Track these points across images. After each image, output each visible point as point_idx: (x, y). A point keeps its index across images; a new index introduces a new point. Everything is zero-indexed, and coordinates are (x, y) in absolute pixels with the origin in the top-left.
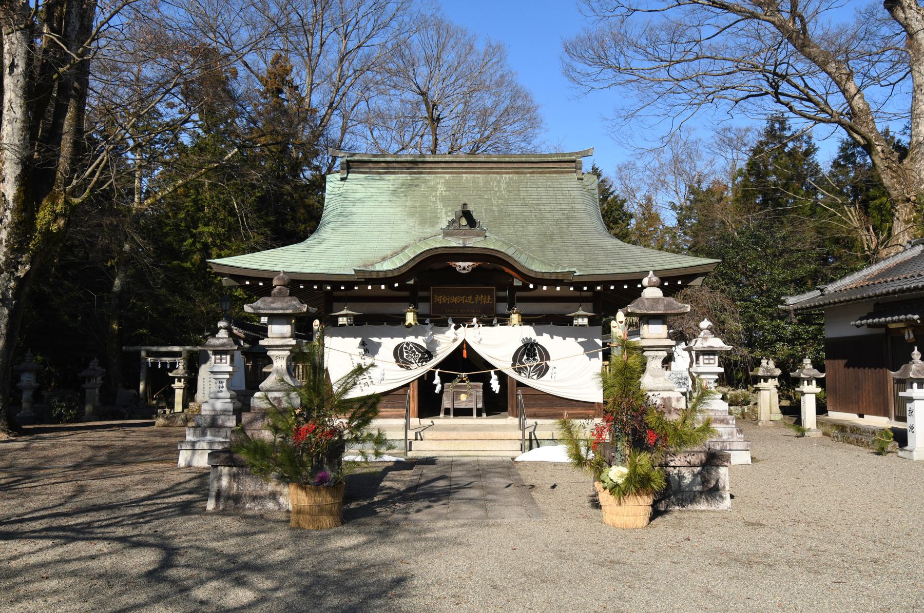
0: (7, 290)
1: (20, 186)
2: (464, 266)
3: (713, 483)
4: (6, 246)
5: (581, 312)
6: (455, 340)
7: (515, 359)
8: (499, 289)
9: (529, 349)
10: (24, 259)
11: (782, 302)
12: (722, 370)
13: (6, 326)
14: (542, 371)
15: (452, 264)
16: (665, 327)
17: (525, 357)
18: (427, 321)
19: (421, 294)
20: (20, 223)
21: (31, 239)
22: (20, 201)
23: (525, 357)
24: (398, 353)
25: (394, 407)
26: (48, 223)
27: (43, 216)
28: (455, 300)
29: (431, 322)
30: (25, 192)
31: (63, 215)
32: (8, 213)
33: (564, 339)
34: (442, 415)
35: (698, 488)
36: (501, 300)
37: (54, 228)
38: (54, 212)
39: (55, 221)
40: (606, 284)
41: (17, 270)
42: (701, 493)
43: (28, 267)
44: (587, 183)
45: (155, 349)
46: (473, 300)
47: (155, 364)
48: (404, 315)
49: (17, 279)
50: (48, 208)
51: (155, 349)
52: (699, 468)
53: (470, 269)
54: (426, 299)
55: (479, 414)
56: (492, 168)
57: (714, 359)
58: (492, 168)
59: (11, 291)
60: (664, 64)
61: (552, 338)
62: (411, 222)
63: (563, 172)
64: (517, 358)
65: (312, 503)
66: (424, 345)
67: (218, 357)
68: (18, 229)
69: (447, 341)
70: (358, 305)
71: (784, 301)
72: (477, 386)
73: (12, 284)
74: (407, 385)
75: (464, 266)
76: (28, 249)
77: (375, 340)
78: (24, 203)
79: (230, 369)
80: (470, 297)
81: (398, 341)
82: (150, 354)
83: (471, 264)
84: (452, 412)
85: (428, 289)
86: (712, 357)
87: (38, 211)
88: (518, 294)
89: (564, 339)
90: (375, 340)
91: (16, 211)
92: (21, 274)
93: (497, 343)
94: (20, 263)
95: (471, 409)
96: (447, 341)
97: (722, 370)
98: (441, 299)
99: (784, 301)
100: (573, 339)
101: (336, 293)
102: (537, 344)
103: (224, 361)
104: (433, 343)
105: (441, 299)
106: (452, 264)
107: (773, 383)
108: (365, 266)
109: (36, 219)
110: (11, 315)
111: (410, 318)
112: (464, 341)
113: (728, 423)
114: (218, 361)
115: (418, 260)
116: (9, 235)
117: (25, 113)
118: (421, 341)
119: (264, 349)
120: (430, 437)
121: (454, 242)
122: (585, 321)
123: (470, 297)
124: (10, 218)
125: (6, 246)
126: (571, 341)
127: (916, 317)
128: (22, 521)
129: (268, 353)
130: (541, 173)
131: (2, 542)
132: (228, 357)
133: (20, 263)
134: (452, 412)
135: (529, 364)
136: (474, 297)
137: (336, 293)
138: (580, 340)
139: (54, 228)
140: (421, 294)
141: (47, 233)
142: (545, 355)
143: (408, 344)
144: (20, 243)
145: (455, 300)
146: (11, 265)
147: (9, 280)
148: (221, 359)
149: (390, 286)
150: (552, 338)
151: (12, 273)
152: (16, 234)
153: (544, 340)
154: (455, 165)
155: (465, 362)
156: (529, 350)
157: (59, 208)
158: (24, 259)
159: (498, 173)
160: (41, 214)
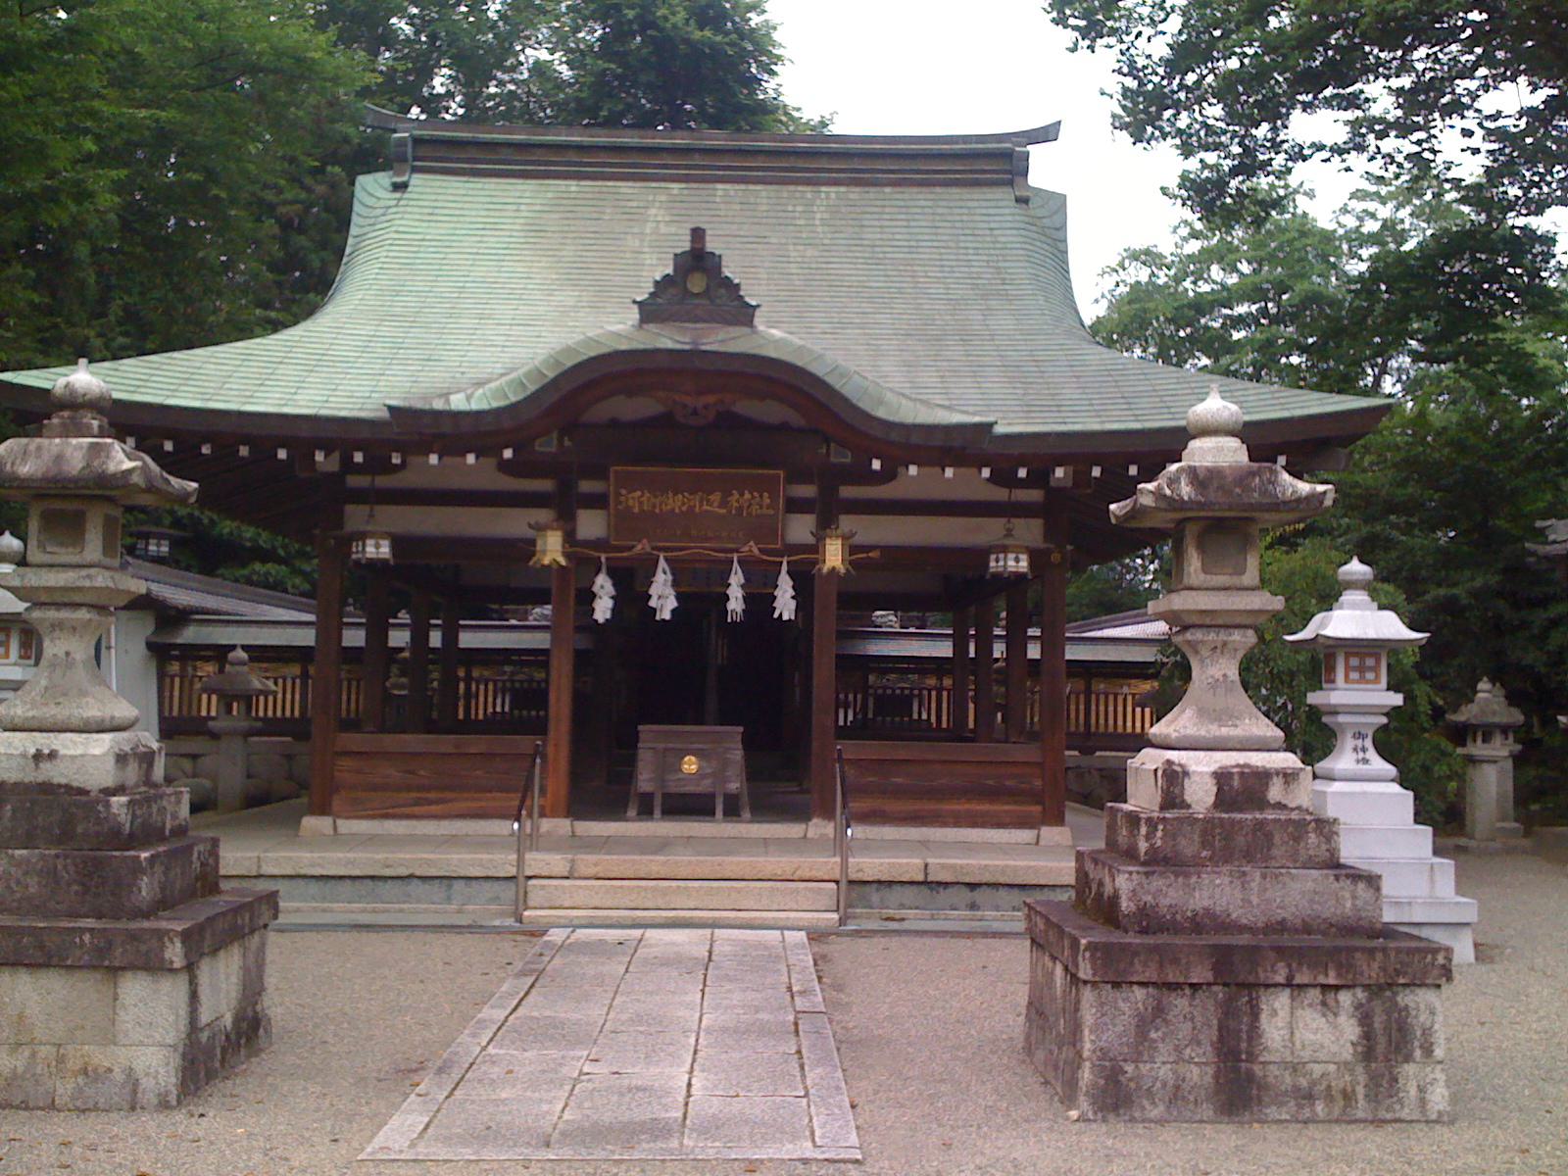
8: (794, 478)
11: (1540, 535)
12: (1397, 699)
19: (586, 486)
28: (675, 503)
34: (632, 813)
36: (795, 506)
44: (1040, 213)
46: (724, 504)
54: (597, 501)
55: (732, 811)
62: (567, 297)
71: (1542, 531)
80: (716, 497)
84: (658, 802)
85: (601, 474)
88: (847, 492)
95: (712, 796)
98: (637, 500)
99: (1542, 531)
107: (1501, 749)
108: (424, 398)
120: (592, 871)
123: (716, 497)
128: (766, 842)
131: (35, 996)
134: (658, 802)
136: (727, 494)
140: (586, 486)
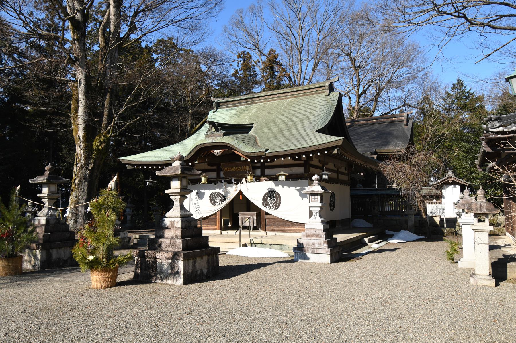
0: (86, 175)
1: (85, 132)
2: (217, 152)
3: (176, 270)
5: (282, 173)
6: (236, 190)
7: (263, 199)
9: (272, 194)
13: (87, 190)
14: (277, 206)
15: (212, 151)
17: (269, 198)
18: (223, 181)
21: (92, 153)
23: (269, 198)
24: (211, 197)
25: (211, 225)
26: (98, 146)
27: (95, 143)
28: (233, 169)
29: (225, 181)
33: (289, 188)
35: (170, 271)
37: (100, 148)
38: (100, 141)
39: (100, 145)
40: (148, 166)
42: (171, 274)
46: (241, 169)
48: (201, 179)
49: (89, 170)
52: (170, 260)
53: (220, 153)
56: (283, 96)
57: (318, 198)
58: (283, 96)
60: (457, 9)
61: (283, 187)
63: (319, 93)
64: (264, 199)
66: (223, 193)
67: (313, 197)
69: (232, 191)
70: (287, 169)
72: (254, 214)
73: (88, 172)
74: (215, 214)
75: (217, 152)
76: (92, 158)
77: (202, 191)
78: (86, 139)
79: (320, 205)
80: (240, 168)
81: (212, 191)
83: (220, 151)
86: (316, 197)
87: (93, 142)
89: (289, 188)
90: (202, 191)
91: (84, 142)
92: (90, 168)
93: (254, 190)
94: (90, 163)
96: (232, 191)
98: (228, 169)
100: (294, 188)
101: (266, 164)
102: (275, 191)
103: (316, 200)
104: (227, 192)
105: (228, 169)
106: (212, 151)
110: (89, 185)
111: (203, 180)
112: (240, 191)
113: (321, 237)
114: (313, 200)
115: (195, 151)
116: (84, 152)
117: (86, 102)
118: (221, 191)
119: (168, 195)
121: (209, 141)
122: (283, 178)
123: (240, 168)
126: (293, 188)
129: (171, 197)
130: (307, 95)
132: (319, 197)
133: (90, 163)
135: (271, 202)
136: (241, 167)
137: (266, 164)
138: (298, 188)
139: (100, 148)
141: (98, 150)
142: (279, 198)
143: (215, 193)
145: (233, 169)
147: (87, 171)
148: (315, 199)
149: (293, 158)
150: (283, 187)
153: (279, 189)
154: (266, 97)
155: (242, 203)
156: (270, 194)
157: (102, 139)
159: (285, 99)
160: (95, 143)
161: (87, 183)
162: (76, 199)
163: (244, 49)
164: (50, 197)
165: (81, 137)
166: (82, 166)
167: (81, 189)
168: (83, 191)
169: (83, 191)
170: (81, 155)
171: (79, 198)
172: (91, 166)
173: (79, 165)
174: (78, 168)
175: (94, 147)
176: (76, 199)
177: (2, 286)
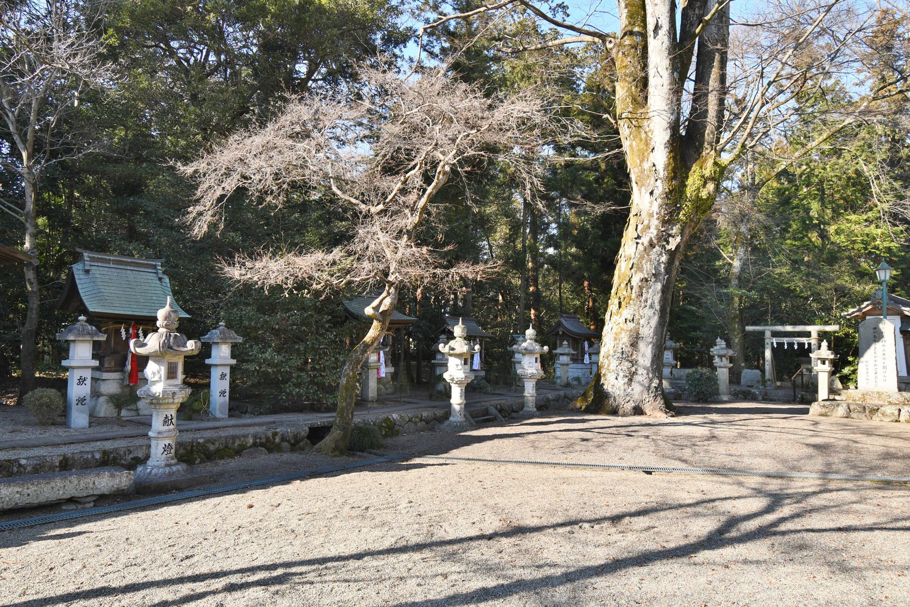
0: (659, 264)
1: (671, 152)
4: (658, 219)
10: (674, 231)
16: (881, 326)
20: (671, 192)
21: (680, 209)
22: (670, 168)
27: (693, 181)
30: (674, 158)
31: (712, 179)
32: (659, 183)
38: (703, 176)
39: (704, 185)
41: (668, 243)
43: (678, 239)
45: (779, 328)
47: (791, 345)
50: (697, 174)
51: (779, 328)
59: (663, 266)
65: (199, 344)
68: (668, 199)
76: (678, 221)
78: (674, 170)
82: (775, 334)
87: (687, 178)
92: (672, 246)
97: (234, 362)
109: (686, 186)
124: (661, 189)
125: (658, 219)
127: (37, 375)
133: (670, 235)
144: (671, 214)
146: (664, 238)
151: (663, 247)
152: (667, 204)
158: (674, 231)
161: (659, 286)
162: (631, 325)
163: (890, 6)
164: (181, 428)
165: (660, 166)
166: (651, 241)
167: (646, 301)
168: (651, 307)
169: (651, 307)
170: (651, 215)
171: (642, 322)
172: (673, 244)
173: (645, 240)
174: (640, 247)
175: (689, 191)
176: (631, 325)
177: (3, 523)
